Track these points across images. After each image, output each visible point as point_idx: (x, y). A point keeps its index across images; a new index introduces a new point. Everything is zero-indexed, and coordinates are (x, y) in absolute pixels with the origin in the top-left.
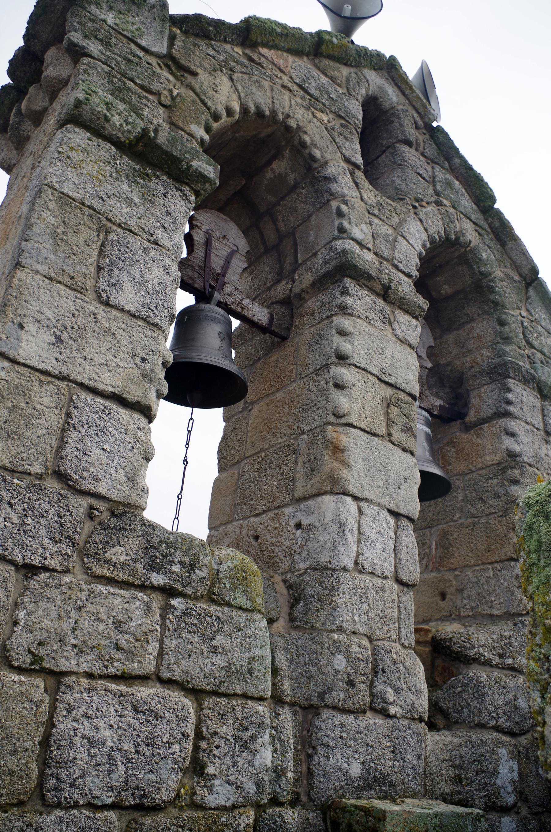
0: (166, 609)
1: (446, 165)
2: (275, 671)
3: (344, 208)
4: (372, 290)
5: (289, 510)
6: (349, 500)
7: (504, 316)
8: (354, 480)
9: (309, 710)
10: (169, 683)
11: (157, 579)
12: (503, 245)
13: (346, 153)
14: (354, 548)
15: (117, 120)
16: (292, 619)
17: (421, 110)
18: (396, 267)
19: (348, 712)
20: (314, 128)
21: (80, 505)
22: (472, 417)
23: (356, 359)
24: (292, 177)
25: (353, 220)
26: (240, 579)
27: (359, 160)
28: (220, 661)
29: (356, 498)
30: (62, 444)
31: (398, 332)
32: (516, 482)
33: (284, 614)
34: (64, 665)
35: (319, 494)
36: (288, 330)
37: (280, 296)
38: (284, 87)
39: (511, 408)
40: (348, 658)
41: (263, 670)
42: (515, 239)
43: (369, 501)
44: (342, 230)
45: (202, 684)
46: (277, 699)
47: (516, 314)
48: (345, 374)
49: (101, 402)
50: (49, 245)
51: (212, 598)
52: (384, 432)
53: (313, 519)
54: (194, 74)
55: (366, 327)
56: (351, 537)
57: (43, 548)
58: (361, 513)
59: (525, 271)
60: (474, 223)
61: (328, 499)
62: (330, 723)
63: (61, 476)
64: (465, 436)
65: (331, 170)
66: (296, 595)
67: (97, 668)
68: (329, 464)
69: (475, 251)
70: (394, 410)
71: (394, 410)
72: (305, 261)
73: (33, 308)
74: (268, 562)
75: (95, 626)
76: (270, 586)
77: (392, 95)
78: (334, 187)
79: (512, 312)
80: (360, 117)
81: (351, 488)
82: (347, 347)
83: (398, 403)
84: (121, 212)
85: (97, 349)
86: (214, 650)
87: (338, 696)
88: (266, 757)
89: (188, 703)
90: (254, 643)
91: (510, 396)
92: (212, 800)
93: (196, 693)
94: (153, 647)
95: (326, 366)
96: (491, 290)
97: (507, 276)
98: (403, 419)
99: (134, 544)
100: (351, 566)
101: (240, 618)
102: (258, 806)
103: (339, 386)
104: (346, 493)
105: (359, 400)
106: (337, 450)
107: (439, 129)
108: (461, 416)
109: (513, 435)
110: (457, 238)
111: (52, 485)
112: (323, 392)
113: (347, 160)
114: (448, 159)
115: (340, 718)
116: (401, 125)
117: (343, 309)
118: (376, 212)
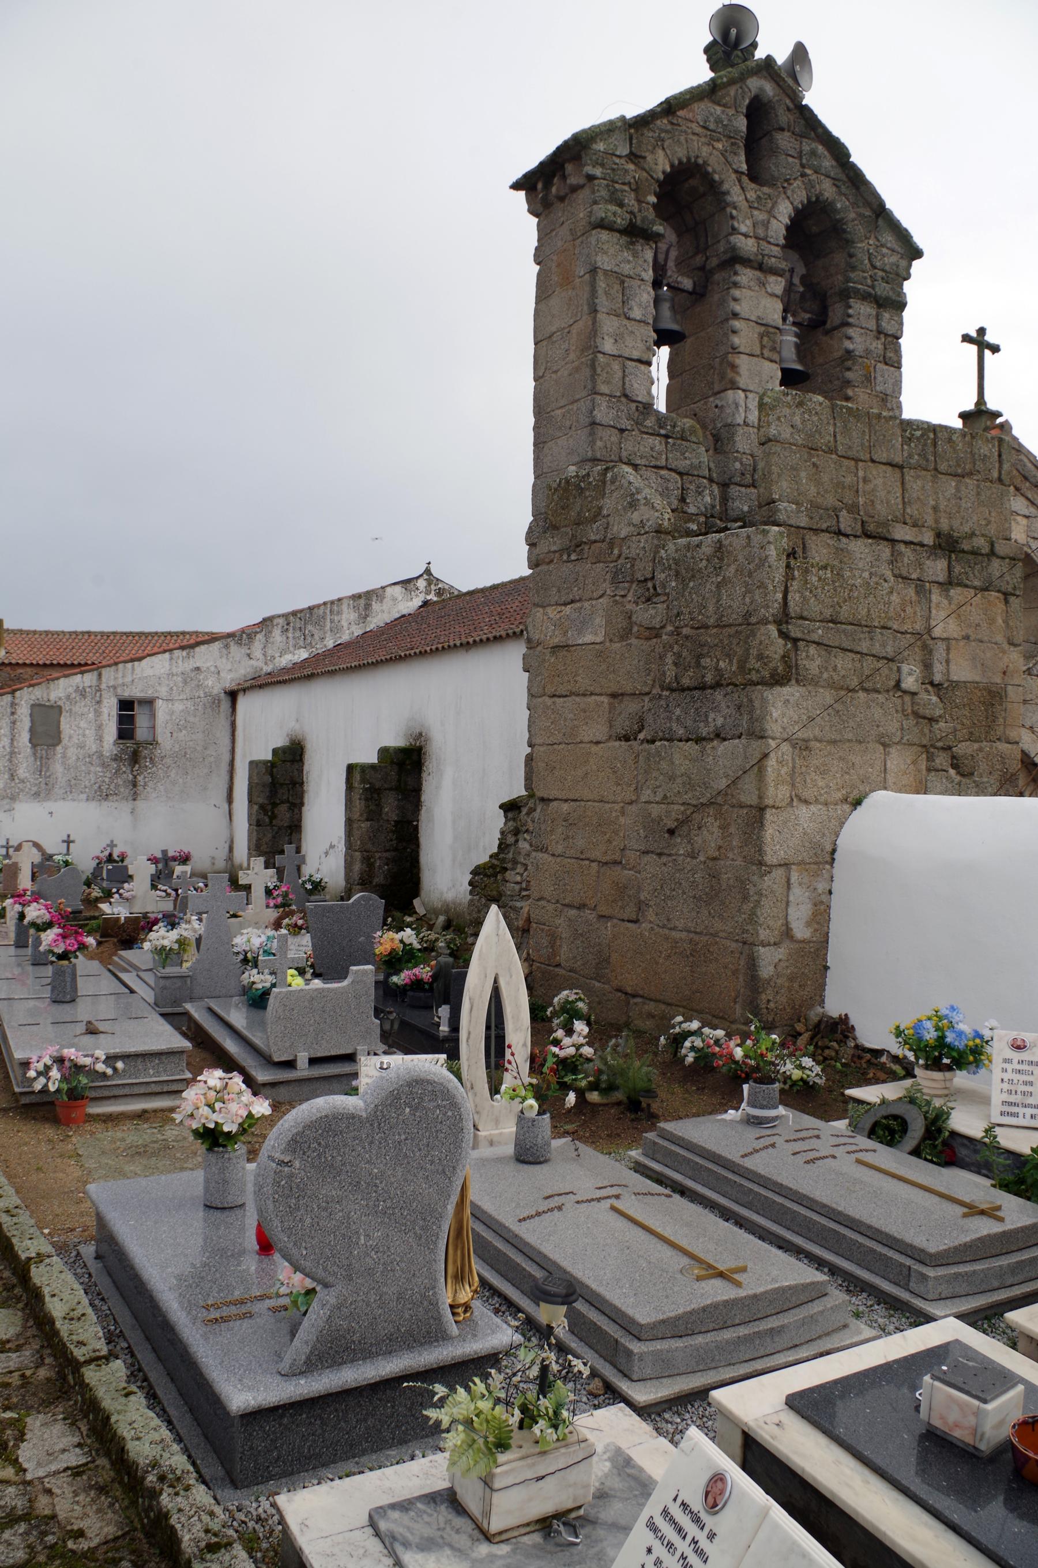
0: (667, 443)
1: (813, 134)
2: (710, 470)
3: (734, 212)
4: (752, 268)
5: (711, 399)
6: (740, 392)
7: (852, 250)
8: (742, 382)
9: (725, 486)
10: (670, 470)
11: (663, 432)
12: (858, 188)
13: (734, 167)
14: (743, 415)
15: (619, 221)
16: (716, 449)
17: (792, 95)
18: (769, 243)
19: (742, 486)
20: (715, 164)
21: (633, 405)
22: (828, 326)
23: (743, 315)
24: (702, 189)
25: (741, 219)
26: (693, 431)
27: (744, 167)
28: (688, 462)
29: (744, 390)
30: (624, 383)
31: (769, 290)
32: (849, 369)
33: (712, 447)
34: (639, 462)
35: (726, 390)
36: (706, 287)
37: (698, 265)
38: (694, 134)
39: (851, 320)
40: (741, 463)
41: (704, 466)
42: (867, 184)
43: (751, 391)
44: (734, 229)
45: (682, 470)
46: (711, 480)
47: (863, 246)
48: (737, 324)
49: (634, 364)
50: (604, 298)
51: (683, 439)
52: (759, 353)
53: (724, 403)
54: (644, 158)
55: (749, 293)
56: (741, 410)
57: (625, 424)
58: (746, 397)
59: (875, 207)
60: (833, 179)
61: (730, 392)
62: (734, 490)
63: (626, 396)
64: (824, 338)
65: (725, 187)
66: (717, 438)
67: (647, 463)
68: (730, 374)
69: (832, 204)
70: (765, 339)
71: (765, 339)
72: (713, 244)
73: (605, 329)
74: (704, 427)
75: (644, 450)
76: (705, 436)
77: (769, 89)
78: (729, 199)
79: (859, 245)
80: (744, 129)
81: (741, 386)
82: (737, 308)
83: (767, 334)
84: (626, 269)
85: (629, 341)
86: (686, 458)
87: (737, 479)
88: (708, 499)
89: (678, 477)
90: (701, 456)
91: (850, 311)
92: (689, 511)
93: (681, 474)
94: (664, 456)
95: (727, 320)
96: (844, 231)
97: (860, 215)
98: (771, 343)
99: (653, 419)
100: (742, 423)
101: (695, 446)
102: (706, 517)
103: (734, 332)
104: (739, 388)
105: (745, 337)
106: (734, 367)
107: (806, 107)
108: (824, 323)
109: (850, 338)
110: (818, 198)
111: (623, 399)
112: (726, 335)
113: (736, 172)
114: (814, 129)
115: (738, 488)
116: (777, 116)
117: (736, 285)
118: (756, 205)
